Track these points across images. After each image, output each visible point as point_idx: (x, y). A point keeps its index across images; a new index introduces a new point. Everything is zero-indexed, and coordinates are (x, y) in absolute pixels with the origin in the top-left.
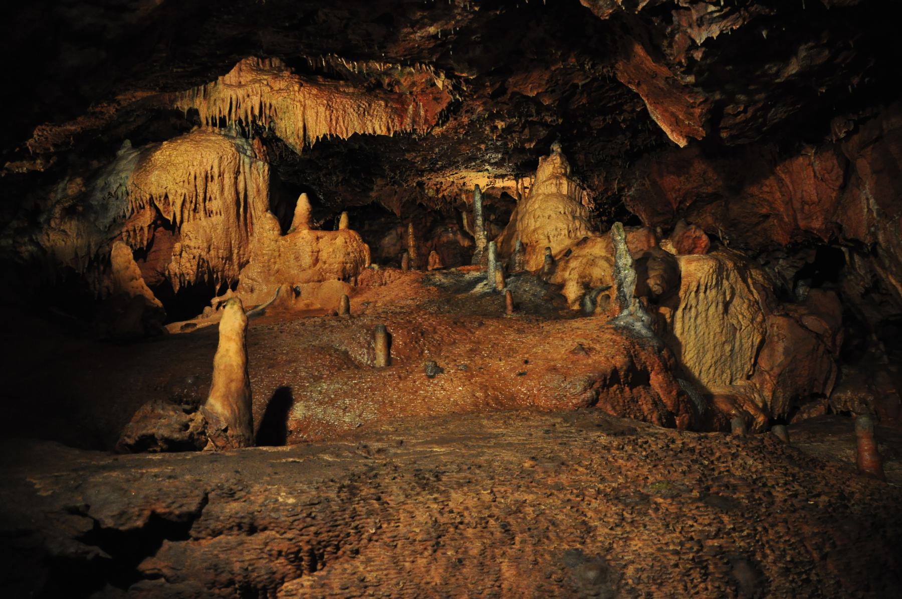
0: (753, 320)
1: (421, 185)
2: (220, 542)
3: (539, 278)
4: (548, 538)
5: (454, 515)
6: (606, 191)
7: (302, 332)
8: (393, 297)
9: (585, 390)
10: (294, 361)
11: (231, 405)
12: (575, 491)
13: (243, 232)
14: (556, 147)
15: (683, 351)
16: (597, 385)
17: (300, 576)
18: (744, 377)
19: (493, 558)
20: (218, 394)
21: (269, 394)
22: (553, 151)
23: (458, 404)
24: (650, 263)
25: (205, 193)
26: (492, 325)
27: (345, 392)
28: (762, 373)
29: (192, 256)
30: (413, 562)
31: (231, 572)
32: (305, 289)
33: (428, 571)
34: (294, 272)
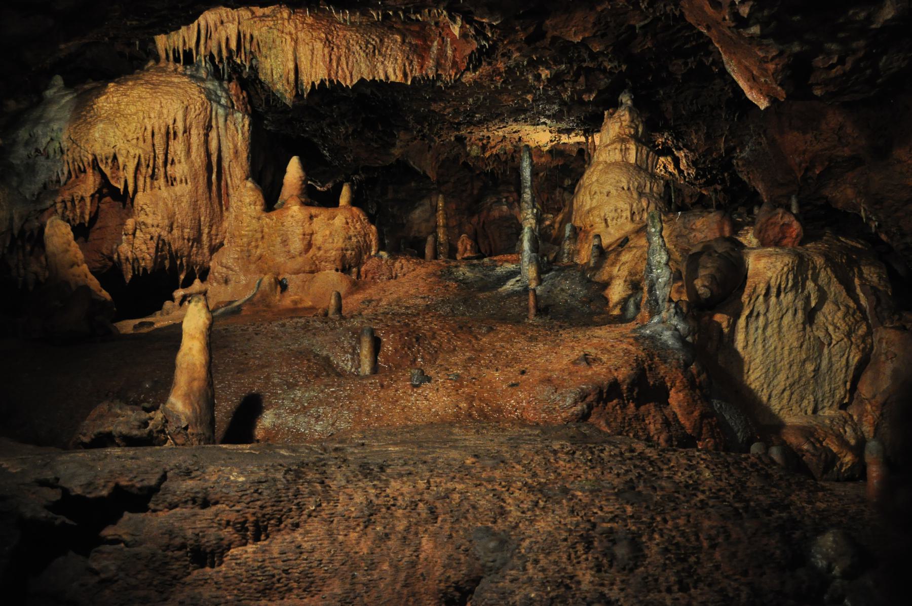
0: (849, 335)
1: (460, 140)
2: (175, 514)
3: (583, 274)
4: (466, 518)
5: (388, 499)
6: (709, 152)
7: (280, 335)
8: (401, 294)
9: (575, 403)
10: (267, 367)
11: (192, 404)
12: (503, 483)
13: (216, 205)
14: (626, 99)
16: (590, 399)
17: (245, 544)
18: (835, 406)
19: (416, 534)
20: (179, 392)
21: (236, 401)
22: (622, 103)
23: (438, 415)
24: (703, 259)
25: (166, 154)
26: (504, 330)
27: (320, 401)
28: (861, 402)
29: (149, 236)
30: (346, 535)
31: (184, 537)
33: (358, 543)
34: (280, 259)
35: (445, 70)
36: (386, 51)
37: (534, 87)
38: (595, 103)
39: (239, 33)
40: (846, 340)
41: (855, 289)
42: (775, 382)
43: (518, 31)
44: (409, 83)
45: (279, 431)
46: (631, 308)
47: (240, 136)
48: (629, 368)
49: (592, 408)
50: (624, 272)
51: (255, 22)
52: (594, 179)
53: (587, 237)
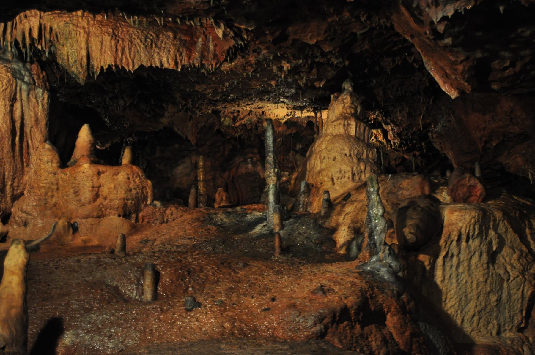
0: (523, 272)
1: (216, 113)
3: (316, 221)
7: (77, 269)
9: (315, 324)
10: (67, 295)
14: (347, 86)
15: (444, 298)
16: (326, 321)
18: (514, 329)
21: (41, 324)
22: (344, 89)
23: (207, 333)
24: (410, 212)
26: (257, 265)
32: (83, 225)
34: (73, 206)
35: (208, 60)
36: (161, 45)
37: (277, 76)
38: (324, 88)
39: (40, 25)
40: (521, 277)
41: (527, 237)
42: (467, 309)
43: (267, 34)
44: (179, 70)
45: (77, 348)
46: (354, 248)
47: (40, 107)
48: (356, 297)
49: (328, 329)
50: (348, 221)
51: (54, 18)
52: (323, 147)
53: (318, 192)
